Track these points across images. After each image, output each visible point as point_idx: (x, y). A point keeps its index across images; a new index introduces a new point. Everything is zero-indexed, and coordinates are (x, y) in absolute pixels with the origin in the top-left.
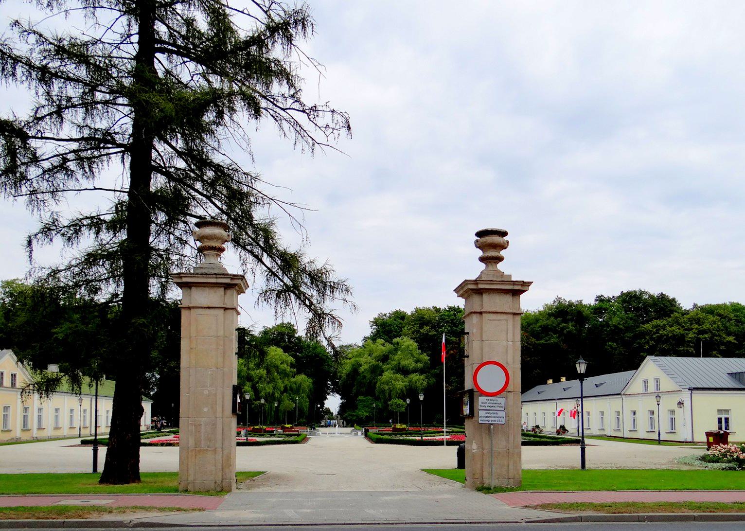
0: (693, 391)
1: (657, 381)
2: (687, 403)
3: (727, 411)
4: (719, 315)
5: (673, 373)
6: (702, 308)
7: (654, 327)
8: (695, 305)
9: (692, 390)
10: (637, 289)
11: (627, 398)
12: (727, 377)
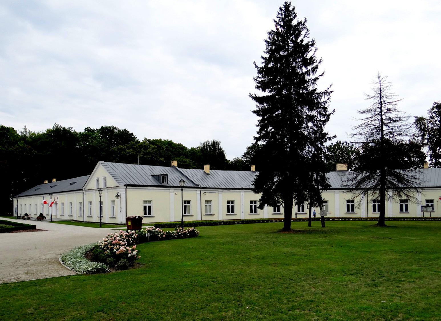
0: (127, 187)
1: (105, 179)
2: (123, 196)
3: (150, 201)
4: (156, 145)
5: (113, 171)
6: (149, 141)
7: (118, 149)
8: (145, 139)
9: (126, 186)
10: (111, 126)
11: (87, 192)
12: (151, 178)
